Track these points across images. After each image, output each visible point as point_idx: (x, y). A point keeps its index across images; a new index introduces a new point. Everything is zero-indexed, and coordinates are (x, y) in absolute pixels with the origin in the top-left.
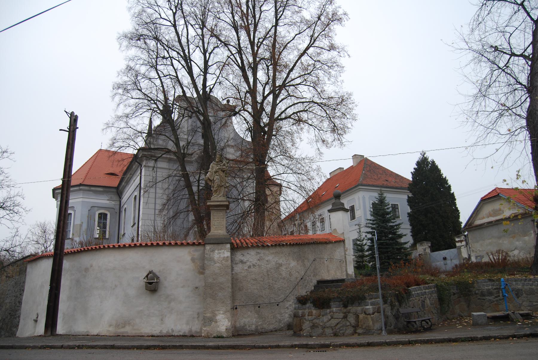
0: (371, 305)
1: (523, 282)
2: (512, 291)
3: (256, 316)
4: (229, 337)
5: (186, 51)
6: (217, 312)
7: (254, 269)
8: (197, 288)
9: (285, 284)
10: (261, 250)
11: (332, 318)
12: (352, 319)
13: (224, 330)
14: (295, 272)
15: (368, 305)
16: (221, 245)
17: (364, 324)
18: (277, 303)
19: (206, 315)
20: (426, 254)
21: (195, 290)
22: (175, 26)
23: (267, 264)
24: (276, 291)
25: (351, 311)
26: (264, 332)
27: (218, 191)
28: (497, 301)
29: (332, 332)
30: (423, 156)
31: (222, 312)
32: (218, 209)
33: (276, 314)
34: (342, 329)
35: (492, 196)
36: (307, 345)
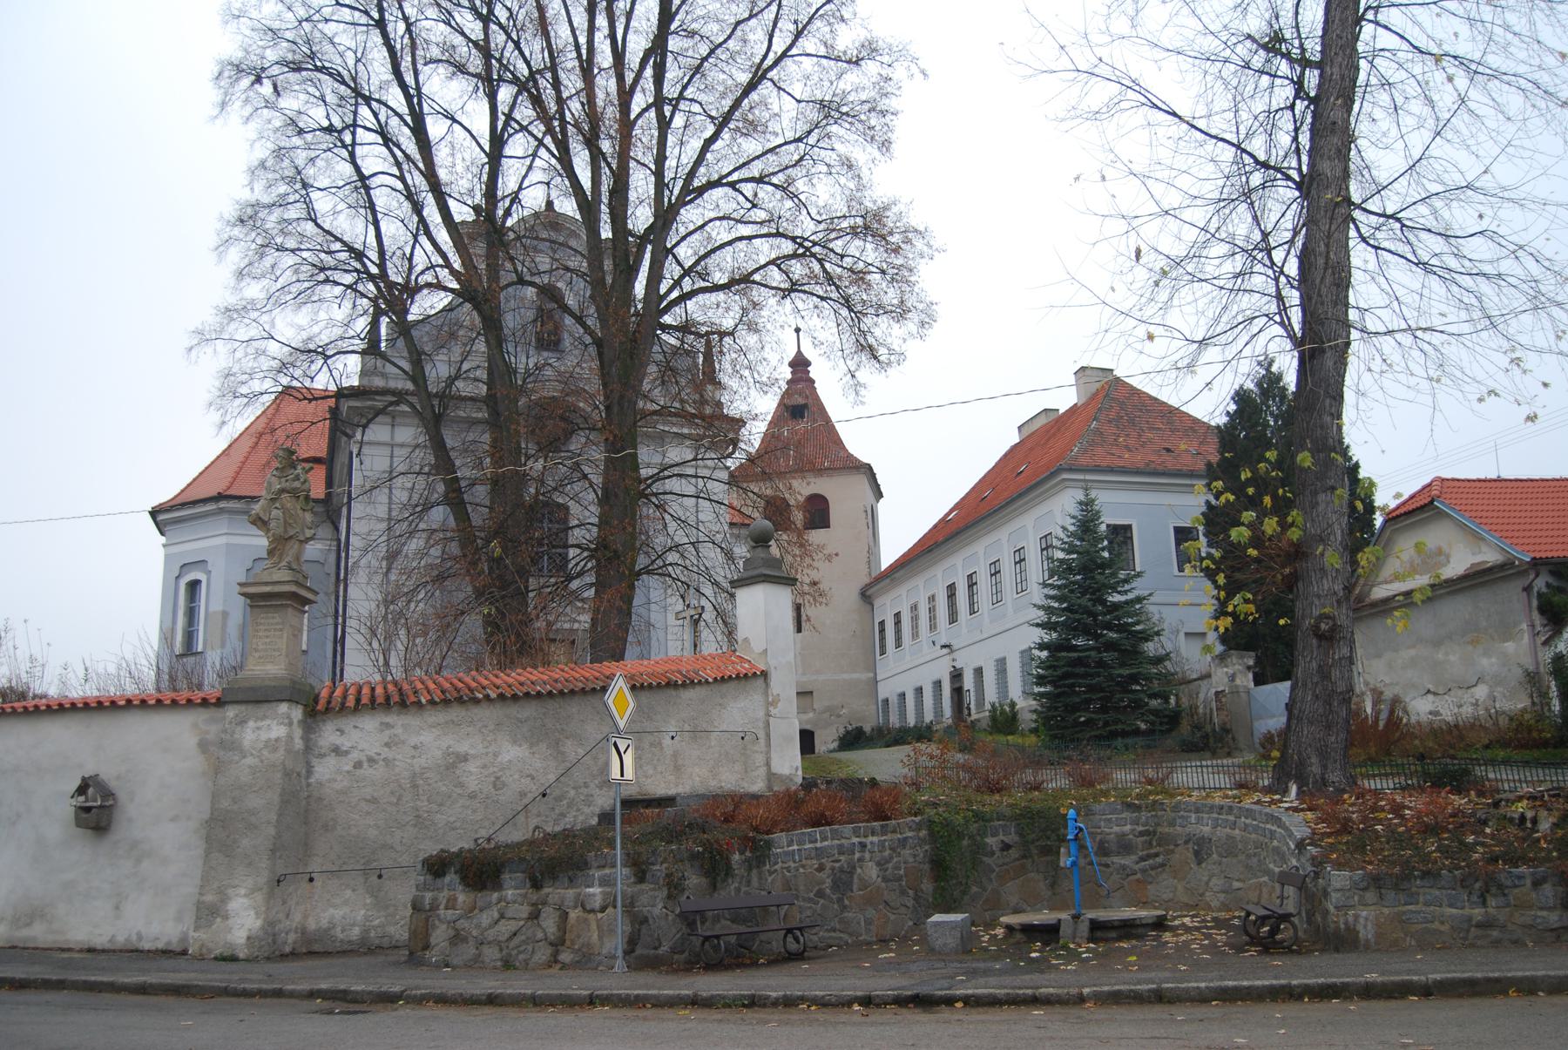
0: (600, 885)
1: (1215, 815)
2: (1186, 842)
3: (368, 901)
7: (371, 771)
9: (474, 811)
11: (502, 916)
12: (549, 923)
13: (243, 941)
14: (516, 776)
15: (591, 886)
16: (265, 706)
17: (579, 937)
20: (1235, 692)
22: (381, 24)
23: (414, 757)
24: (441, 831)
25: (550, 900)
27: (278, 553)
28: (1144, 871)
29: (498, 956)
30: (1268, 369)
31: (243, 891)
34: (522, 949)
35: (1414, 506)
36: (345, 992)
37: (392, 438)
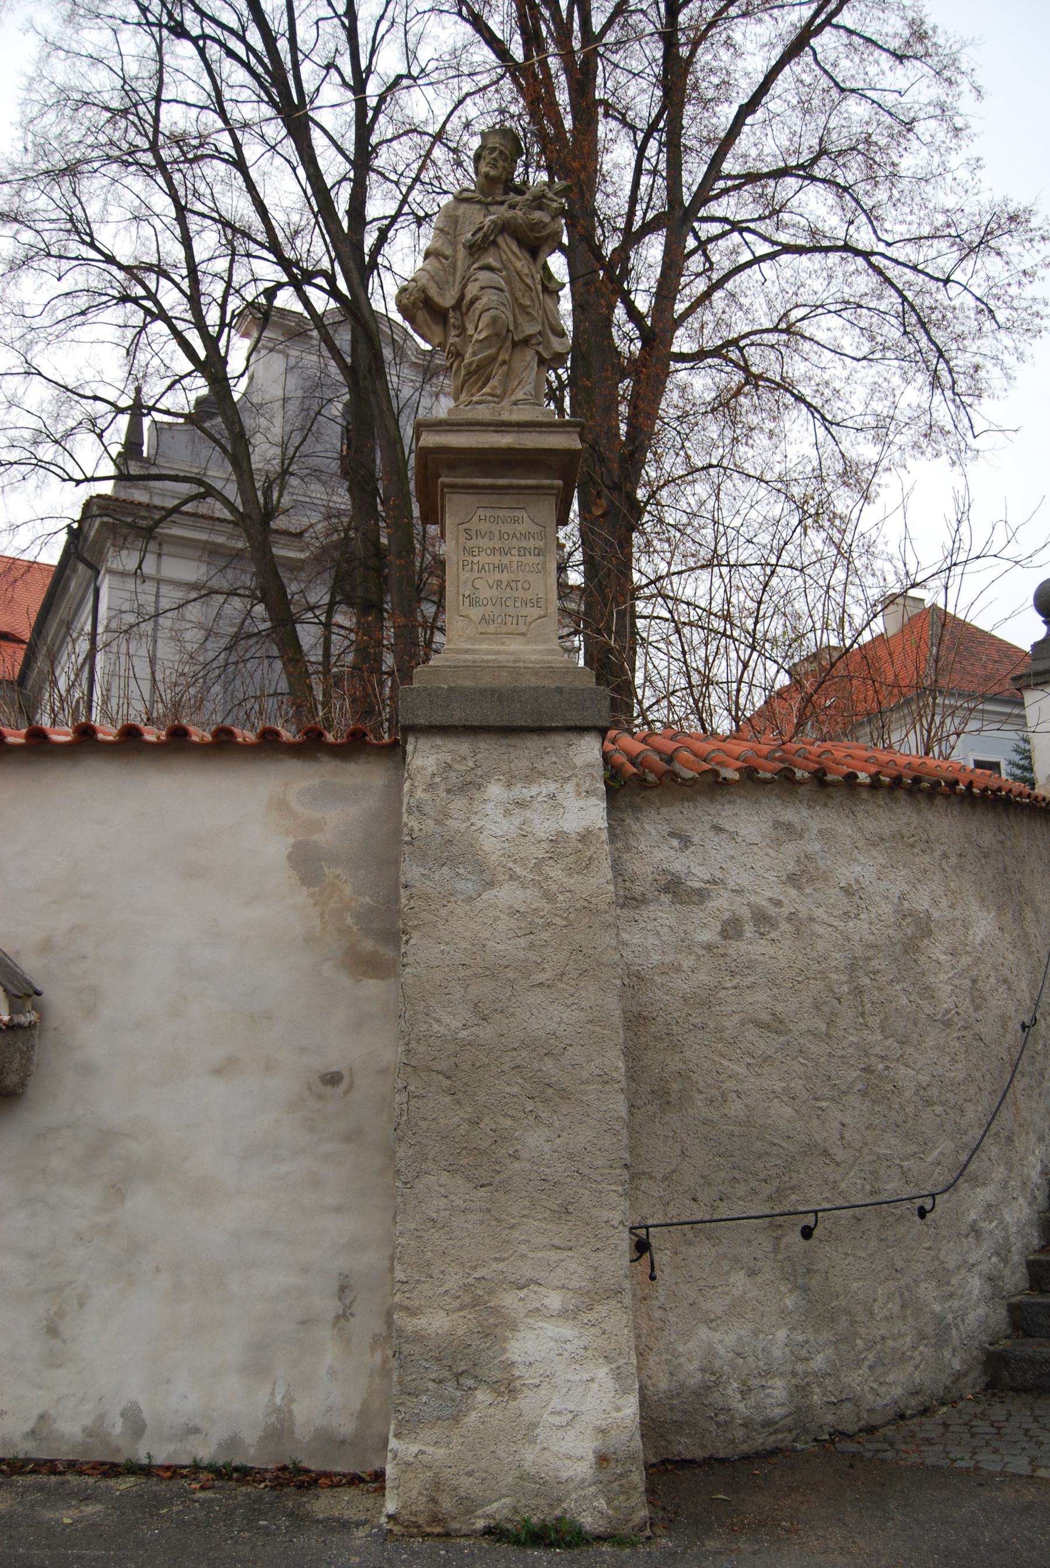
3: (789, 1302)
4: (626, 1530)
5: (283, 45)
6: (509, 1300)
8: (333, 1079)
10: (805, 813)
13: (584, 1469)
14: (992, 980)
16: (534, 744)
18: (919, 1202)
19: (420, 1322)
21: (320, 1097)
24: (910, 1109)
26: (851, 1428)
27: (499, 373)
31: (555, 1301)
32: (501, 482)
33: (916, 1282)
37: (158, 570)
